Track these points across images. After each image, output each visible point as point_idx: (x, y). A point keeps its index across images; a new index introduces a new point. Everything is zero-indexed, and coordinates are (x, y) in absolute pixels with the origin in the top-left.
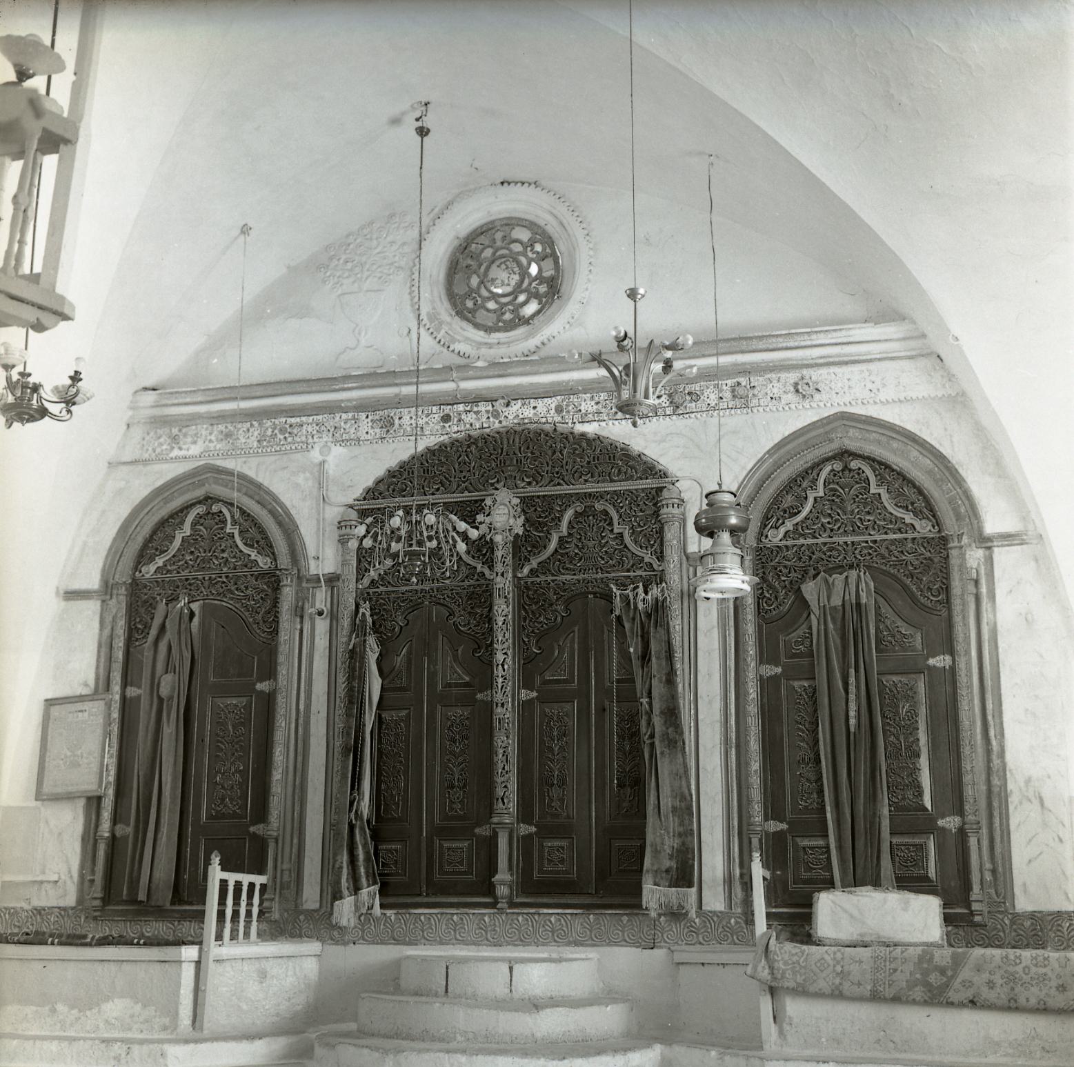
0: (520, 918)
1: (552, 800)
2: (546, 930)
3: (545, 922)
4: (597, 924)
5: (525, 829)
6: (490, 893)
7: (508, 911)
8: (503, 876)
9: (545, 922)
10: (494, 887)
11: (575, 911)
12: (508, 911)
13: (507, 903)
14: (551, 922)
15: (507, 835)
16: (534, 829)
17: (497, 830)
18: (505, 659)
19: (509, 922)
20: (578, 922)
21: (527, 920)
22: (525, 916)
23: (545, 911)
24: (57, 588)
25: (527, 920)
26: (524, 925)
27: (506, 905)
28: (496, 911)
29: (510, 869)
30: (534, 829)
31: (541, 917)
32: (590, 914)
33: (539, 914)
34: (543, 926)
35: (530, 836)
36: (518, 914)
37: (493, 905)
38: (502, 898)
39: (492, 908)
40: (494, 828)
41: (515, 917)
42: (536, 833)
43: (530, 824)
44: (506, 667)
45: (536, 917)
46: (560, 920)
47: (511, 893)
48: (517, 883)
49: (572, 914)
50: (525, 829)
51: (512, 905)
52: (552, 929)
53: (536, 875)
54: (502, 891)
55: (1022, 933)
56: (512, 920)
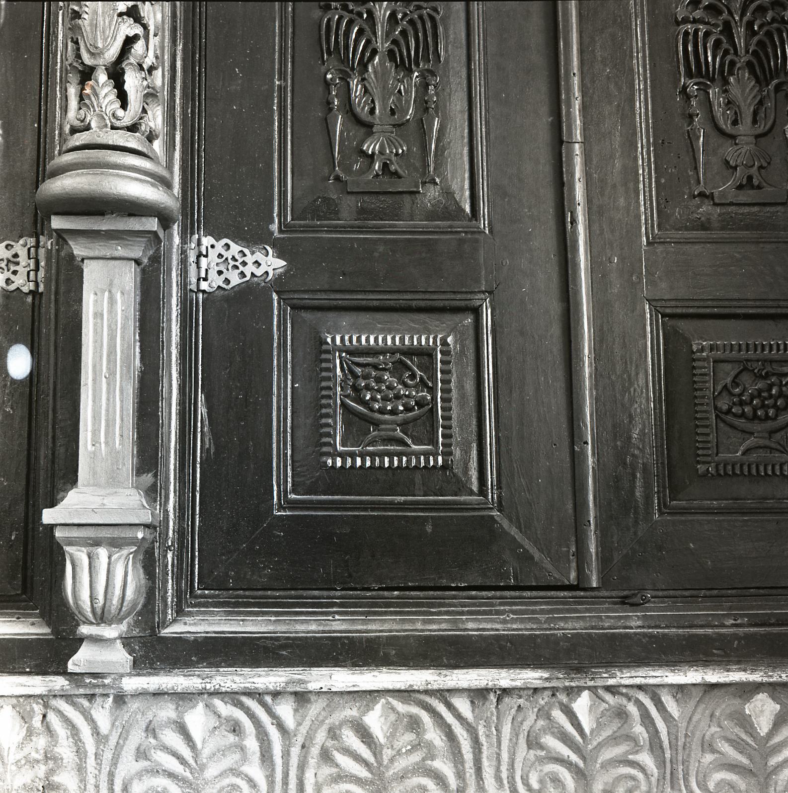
0: (197, 719)
1: (368, 128)
2: (341, 777)
3: (333, 733)
4: (614, 740)
5: (222, 263)
6: (27, 586)
7: (131, 684)
8: (105, 499)
9: (333, 733)
10: (55, 557)
11: (504, 678)
12: (131, 684)
13: (127, 642)
14: (365, 735)
15: (127, 278)
16: (271, 264)
17: (78, 249)
18: (129, 41)
19: (137, 737)
20: (506, 730)
21: (236, 728)
22: (225, 709)
23: (342, 678)
24: (140, 745)
25: (236, 728)
26: (223, 751)
27: (120, 657)
28: (59, 682)
29: (148, 456)
30: (271, 264)
31: (315, 708)
32: (573, 692)
33: (302, 698)
34: (326, 756)
35: (250, 295)
36: (184, 698)
37: (51, 655)
38: (102, 618)
39: (42, 671)
40: (61, 236)
41: (167, 711)
42: (280, 284)
43: (254, 237)
44: (132, 81)
45: (285, 710)
46: (414, 724)
47: (151, 594)
48: (181, 533)
49: (478, 695)
50: (222, 263)
51: (154, 650)
52: (377, 769)
53: (282, 488)
54: (101, 578)
55: (565, 751)
56: (151, 730)
